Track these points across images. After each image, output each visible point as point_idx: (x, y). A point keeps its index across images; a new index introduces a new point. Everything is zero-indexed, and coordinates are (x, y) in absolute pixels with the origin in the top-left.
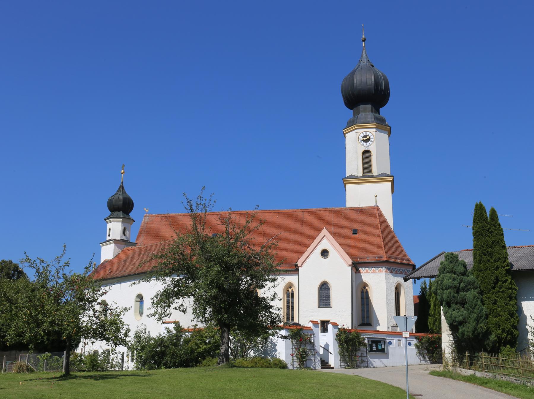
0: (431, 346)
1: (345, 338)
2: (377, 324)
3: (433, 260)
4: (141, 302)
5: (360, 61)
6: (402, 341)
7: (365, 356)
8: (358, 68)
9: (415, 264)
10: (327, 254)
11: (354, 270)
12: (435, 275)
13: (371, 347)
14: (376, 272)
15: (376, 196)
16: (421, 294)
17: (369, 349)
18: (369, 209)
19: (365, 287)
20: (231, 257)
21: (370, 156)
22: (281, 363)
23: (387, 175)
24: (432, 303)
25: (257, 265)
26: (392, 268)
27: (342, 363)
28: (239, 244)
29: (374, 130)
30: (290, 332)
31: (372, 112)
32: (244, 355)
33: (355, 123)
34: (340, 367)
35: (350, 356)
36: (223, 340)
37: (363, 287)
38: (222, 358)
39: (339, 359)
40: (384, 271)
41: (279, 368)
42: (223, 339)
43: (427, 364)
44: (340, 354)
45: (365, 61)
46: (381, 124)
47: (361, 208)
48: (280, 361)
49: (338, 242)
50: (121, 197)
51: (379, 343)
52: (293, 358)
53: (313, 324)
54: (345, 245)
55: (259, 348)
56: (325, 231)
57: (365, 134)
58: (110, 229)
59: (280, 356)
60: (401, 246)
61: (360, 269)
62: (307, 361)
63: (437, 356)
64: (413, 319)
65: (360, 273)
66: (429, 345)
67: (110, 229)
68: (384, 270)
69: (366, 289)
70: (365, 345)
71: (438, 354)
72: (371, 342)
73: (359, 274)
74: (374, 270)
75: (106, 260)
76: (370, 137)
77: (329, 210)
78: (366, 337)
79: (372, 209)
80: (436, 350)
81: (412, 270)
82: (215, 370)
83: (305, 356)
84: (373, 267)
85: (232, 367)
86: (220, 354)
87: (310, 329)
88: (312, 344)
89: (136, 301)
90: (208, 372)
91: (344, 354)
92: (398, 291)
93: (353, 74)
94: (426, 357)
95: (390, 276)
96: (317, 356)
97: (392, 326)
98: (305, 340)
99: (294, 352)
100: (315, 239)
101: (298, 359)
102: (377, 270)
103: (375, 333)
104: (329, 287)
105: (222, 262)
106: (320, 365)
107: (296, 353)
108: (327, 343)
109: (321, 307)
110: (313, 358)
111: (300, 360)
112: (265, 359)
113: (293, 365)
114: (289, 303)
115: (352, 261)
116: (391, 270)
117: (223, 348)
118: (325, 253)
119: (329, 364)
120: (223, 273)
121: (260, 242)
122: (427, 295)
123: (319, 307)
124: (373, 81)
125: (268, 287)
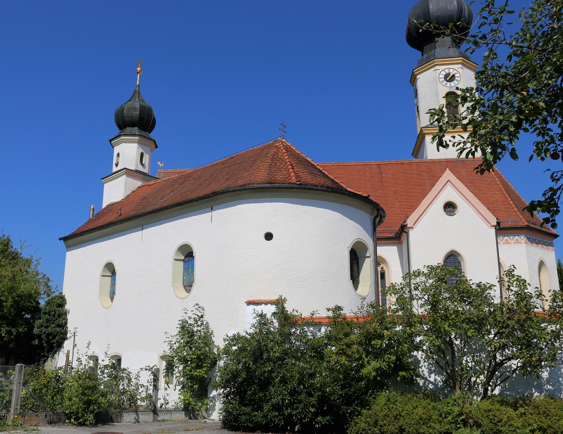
4: (187, 263)
14: (511, 243)
29: (460, 66)
40: (523, 242)
50: (137, 105)
58: (118, 155)
67: (118, 155)
68: (523, 240)
74: (506, 240)
75: (111, 203)
77: (416, 163)
79: (479, 160)
89: (176, 260)
102: (512, 240)
115: (497, 219)
118: (450, 207)
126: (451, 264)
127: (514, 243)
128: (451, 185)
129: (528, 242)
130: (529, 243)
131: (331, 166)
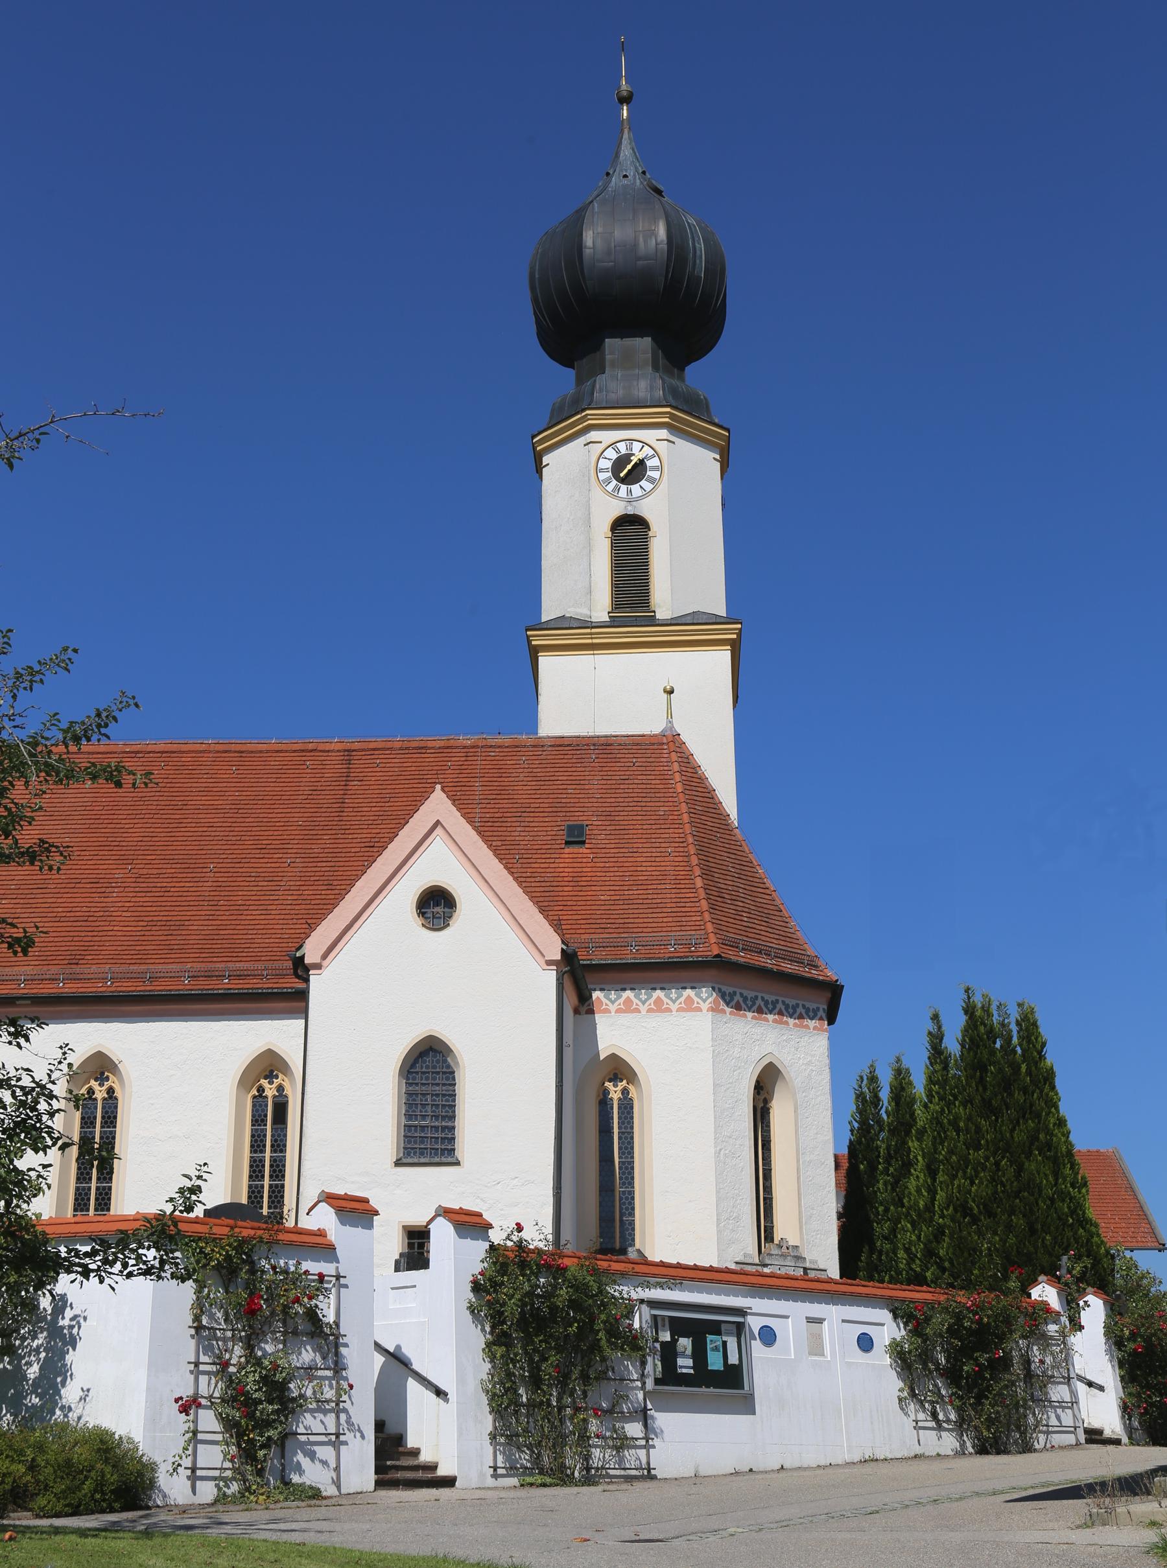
0: (971, 1358)
5: (608, 174)
6: (826, 1323)
9: (841, 982)
10: (446, 910)
11: (571, 1000)
13: (669, 1353)
15: (671, 692)
18: (638, 744)
23: (715, 620)
29: (664, 433)
31: (656, 367)
39: (489, 1428)
40: (705, 1006)
47: (602, 740)
51: (709, 1337)
56: (438, 805)
60: (778, 902)
65: (591, 1012)
68: (704, 1001)
73: (590, 1016)
74: (659, 1001)
77: (465, 747)
87: (316, 1246)
102: (674, 1002)
104: (449, 1066)
115: (563, 942)
121: (145, 871)
124: (662, 241)
126: (427, 1079)
127: (679, 1010)
128: (445, 837)
129: (723, 1005)
130: (728, 1010)
131: (201, 752)
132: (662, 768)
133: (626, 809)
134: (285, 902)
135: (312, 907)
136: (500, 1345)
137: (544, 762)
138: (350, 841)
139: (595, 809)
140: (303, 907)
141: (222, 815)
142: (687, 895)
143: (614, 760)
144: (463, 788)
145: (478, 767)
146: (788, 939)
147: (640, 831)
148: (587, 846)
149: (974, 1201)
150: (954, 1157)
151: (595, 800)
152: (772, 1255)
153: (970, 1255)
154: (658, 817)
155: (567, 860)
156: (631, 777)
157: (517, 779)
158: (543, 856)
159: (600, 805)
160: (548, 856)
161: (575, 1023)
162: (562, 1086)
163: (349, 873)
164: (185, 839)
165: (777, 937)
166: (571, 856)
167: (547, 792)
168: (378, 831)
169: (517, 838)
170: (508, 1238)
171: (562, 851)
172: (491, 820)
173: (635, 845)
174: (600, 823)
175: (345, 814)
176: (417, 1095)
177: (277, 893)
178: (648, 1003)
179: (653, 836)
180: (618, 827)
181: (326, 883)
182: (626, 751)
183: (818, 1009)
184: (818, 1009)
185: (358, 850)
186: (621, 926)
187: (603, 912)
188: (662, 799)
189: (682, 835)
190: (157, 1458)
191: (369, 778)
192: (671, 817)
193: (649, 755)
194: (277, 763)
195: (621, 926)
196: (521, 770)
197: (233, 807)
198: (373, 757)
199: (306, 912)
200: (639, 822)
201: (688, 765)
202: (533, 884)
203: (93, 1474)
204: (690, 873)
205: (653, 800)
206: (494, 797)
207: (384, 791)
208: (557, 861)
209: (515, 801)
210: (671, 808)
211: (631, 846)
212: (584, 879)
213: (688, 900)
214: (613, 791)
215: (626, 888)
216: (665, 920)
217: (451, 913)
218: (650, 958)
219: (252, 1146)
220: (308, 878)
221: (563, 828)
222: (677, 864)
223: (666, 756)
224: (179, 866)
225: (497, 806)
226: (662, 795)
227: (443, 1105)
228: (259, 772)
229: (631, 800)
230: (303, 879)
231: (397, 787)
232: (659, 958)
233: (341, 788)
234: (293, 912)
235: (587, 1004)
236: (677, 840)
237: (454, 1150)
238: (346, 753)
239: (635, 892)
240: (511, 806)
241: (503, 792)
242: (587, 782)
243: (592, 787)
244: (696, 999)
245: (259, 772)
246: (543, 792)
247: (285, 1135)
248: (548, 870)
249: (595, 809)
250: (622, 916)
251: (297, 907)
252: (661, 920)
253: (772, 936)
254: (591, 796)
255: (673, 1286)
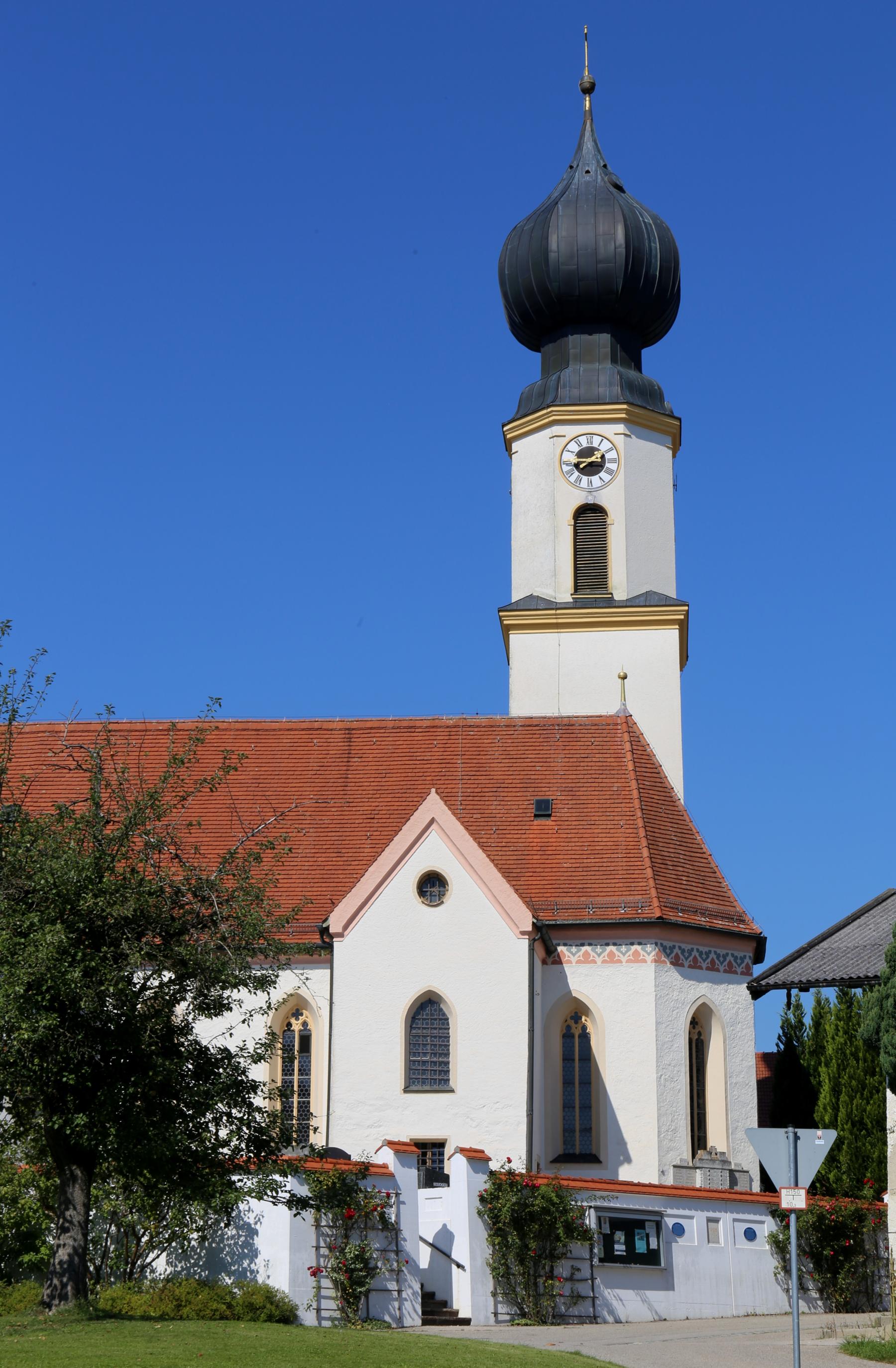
0: (829, 1245)
1: (513, 1210)
2: (622, 1158)
3: (853, 921)
5: (571, 167)
6: (721, 1222)
7: (587, 1280)
8: (563, 194)
9: (765, 934)
10: (442, 889)
11: (540, 952)
12: (867, 977)
13: (608, 1242)
14: (621, 962)
15: (624, 677)
16: (782, 1046)
17: (599, 1252)
18: (596, 725)
19: (576, 1018)
20: (111, 894)
21: (604, 525)
22: (272, 1303)
23: (666, 601)
24: (827, 1081)
25: (207, 923)
26: (680, 948)
27: (500, 1302)
28: (138, 842)
29: (621, 428)
30: (309, 1184)
31: (614, 360)
32: (131, 1270)
33: (549, 400)
34: (492, 1318)
35: (532, 1278)
36: (68, 1213)
37: (572, 1018)
38: (61, 1282)
39: (491, 1288)
40: (650, 958)
41: (266, 1321)
42: (67, 1209)
43: (813, 1310)
44: (494, 1269)
45: (592, 168)
46: (645, 408)
47: (566, 721)
48: (269, 1295)
49: (482, 846)
51: (637, 1231)
52: (319, 1282)
53: (397, 1152)
54: (504, 858)
55: (190, 1243)
57: (585, 444)
59: (269, 1277)
60: (712, 865)
61: (560, 949)
62: (373, 1296)
63: (850, 1284)
64: (822, 1142)
66: (819, 1240)
68: (649, 954)
69: (580, 1026)
70: (585, 1235)
71: (854, 1273)
72: (608, 1225)
73: (559, 966)
74: (611, 954)
76: (603, 457)
77: (448, 727)
78: (592, 1204)
79: (609, 725)
80: (848, 1259)
81: (751, 955)
82: (34, 1331)
83: (366, 1277)
84: (611, 941)
85: (98, 1318)
86: (52, 1268)
87: (383, 1174)
88: (392, 1230)
90: (10, 1339)
91: (508, 1268)
92: (700, 1034)
93: (544, 215)
94: (811, 1285)
95: (673, 975)
96: (409, 1277)
97: (674, 1166)
98: (367, 1215)
99: (322, 1260)
100: (397, 833)
101: (336, 1287)
103: (625, 1192)
104: (444, 1014)
105: (75, 912)
106: (420, 1312)
107: (332, 1263)
108: (445, 1226)
109: (413, 1088)
110: (395, 1283)
111: (344, 1290)
112: (212, 1288)
113: (318, 1310)
114: (292, 1074)
115: (534, 917)
116: (677, 956)
117: (64, 1245)
119: (451, 1307)
120: (76, 954)
122: (803, 1052)
123: (407, 1090)
124: (620, 246)
125: (243, 1010)
126: (427, 1024)
128: (440, 831)
132: (616, 747)
133: (586, 785)
134: (303, 868)
135: (325, 872)
136: (498, 1236)
137: (516, 741)
138: (354, 813)
139: (559, 785)
140: (318, 872)
141: (245, 789)
142: (636, 864)
143: (575, 739)
144: (448, 765)
145: (460, 745)
146: (721, 898)
147: (597, 806)
148: (552, 818)
149: (868, 1117)
150: (853, 1081)
151: (559, 777)
152: (703, 1160)
153: (864, 1161)
154: (612, 793)
155: (536, 832)
156: (590, 756)
157: (493, 757)
158: (516, 828)
159: (563, 781)
160: (520, 827)
161: (543, 972)
162: (533, 1031)
163: (355, 842)
164: (216, 810)
165: (711, 896)
166: (539, 827)
167: (518, 769)
168: (377, 804)
169: (494, 811)
170: (502, 1167)
171: (531, 823)
172: (472, 794)
173: (593, 818)
174: (563, 798)
175: (349, 788)
176: (419, 1036)
177: (296, 859)
178: (603, 955)
179: (608, 810)
180: (578, 802)
181: (336, 850)
182: (586, 731)
183: (745, 956)
184: (745, 956)
185: (361, 821)
186: (581, 890)
187: (566, 878)
188: (616, 776)
189: (632, 809)
190: (297, 1301)
191: (368, 755)
192: (623, 793)
193: (605, 735)
194: (289, 741)
195: (581, 890)
196: (496, 749)
197: (254, 781)
198: (369, 735)
199: (321, 876)
200: (597, 797)
201: (638, 744)
202: (508, 853)
203: (265, 1310)
204: (638, 843)
205: (608, 776)
206: (474, 773)
207: (380, 768)
208: (528, 832)
209: (491, 777)
210: (624, 785)
211: (588, 818)
212: (550, 848)
213: (636, 868)
214: (575, 768)
215: (585, 857)
216: (617, 885)
217: (444, 891)
218: (604, 919)
219: (283, 1070)
220: (321, 847)
221: (532, 802)
222: (628, 835)
223: (620, 735)
224: (213, 835)
225: (476, 782)
226: (615, 772)
227: (439, 1045)
228: (274, 749)
229: (589, 776)
230: (316, 847)
231: (392, 763)
232: (612, 919)
233: (345, 764)
234: (310, 876)
235: (553, 955)
236: (628, 813)
237: (449, 1080)
238: (347, 732)
239: (593, 861)
240: (488, 781)
241: (481, 769)
242: (552, 760)
243: (556, 764)
244: (642, 952)
245: (274, 749)
246: (515, 769)
247: (310, 1062)
248: (520, 840)
249: (559, 785)
250: (581, 882)
251: (313, 872)
252: (613, 885)
253: (707, 896)
254: (556, 772)
255: (611, 1199)
